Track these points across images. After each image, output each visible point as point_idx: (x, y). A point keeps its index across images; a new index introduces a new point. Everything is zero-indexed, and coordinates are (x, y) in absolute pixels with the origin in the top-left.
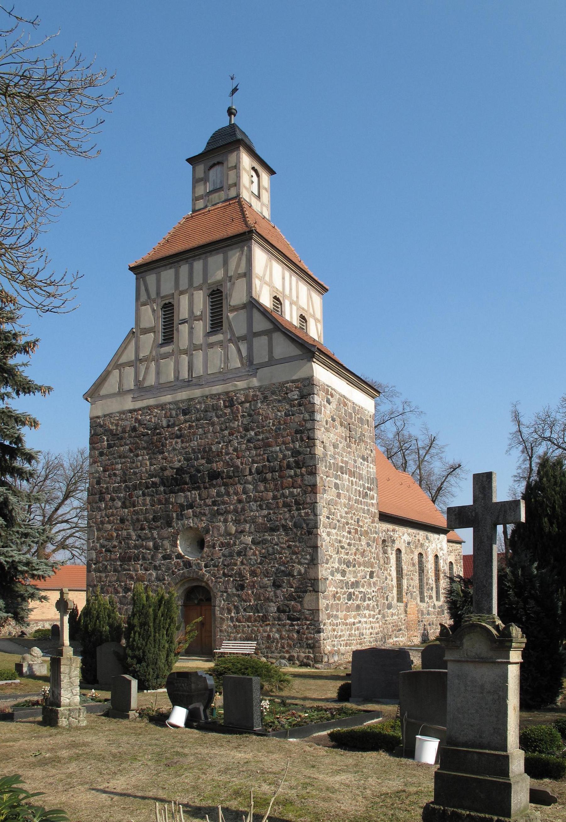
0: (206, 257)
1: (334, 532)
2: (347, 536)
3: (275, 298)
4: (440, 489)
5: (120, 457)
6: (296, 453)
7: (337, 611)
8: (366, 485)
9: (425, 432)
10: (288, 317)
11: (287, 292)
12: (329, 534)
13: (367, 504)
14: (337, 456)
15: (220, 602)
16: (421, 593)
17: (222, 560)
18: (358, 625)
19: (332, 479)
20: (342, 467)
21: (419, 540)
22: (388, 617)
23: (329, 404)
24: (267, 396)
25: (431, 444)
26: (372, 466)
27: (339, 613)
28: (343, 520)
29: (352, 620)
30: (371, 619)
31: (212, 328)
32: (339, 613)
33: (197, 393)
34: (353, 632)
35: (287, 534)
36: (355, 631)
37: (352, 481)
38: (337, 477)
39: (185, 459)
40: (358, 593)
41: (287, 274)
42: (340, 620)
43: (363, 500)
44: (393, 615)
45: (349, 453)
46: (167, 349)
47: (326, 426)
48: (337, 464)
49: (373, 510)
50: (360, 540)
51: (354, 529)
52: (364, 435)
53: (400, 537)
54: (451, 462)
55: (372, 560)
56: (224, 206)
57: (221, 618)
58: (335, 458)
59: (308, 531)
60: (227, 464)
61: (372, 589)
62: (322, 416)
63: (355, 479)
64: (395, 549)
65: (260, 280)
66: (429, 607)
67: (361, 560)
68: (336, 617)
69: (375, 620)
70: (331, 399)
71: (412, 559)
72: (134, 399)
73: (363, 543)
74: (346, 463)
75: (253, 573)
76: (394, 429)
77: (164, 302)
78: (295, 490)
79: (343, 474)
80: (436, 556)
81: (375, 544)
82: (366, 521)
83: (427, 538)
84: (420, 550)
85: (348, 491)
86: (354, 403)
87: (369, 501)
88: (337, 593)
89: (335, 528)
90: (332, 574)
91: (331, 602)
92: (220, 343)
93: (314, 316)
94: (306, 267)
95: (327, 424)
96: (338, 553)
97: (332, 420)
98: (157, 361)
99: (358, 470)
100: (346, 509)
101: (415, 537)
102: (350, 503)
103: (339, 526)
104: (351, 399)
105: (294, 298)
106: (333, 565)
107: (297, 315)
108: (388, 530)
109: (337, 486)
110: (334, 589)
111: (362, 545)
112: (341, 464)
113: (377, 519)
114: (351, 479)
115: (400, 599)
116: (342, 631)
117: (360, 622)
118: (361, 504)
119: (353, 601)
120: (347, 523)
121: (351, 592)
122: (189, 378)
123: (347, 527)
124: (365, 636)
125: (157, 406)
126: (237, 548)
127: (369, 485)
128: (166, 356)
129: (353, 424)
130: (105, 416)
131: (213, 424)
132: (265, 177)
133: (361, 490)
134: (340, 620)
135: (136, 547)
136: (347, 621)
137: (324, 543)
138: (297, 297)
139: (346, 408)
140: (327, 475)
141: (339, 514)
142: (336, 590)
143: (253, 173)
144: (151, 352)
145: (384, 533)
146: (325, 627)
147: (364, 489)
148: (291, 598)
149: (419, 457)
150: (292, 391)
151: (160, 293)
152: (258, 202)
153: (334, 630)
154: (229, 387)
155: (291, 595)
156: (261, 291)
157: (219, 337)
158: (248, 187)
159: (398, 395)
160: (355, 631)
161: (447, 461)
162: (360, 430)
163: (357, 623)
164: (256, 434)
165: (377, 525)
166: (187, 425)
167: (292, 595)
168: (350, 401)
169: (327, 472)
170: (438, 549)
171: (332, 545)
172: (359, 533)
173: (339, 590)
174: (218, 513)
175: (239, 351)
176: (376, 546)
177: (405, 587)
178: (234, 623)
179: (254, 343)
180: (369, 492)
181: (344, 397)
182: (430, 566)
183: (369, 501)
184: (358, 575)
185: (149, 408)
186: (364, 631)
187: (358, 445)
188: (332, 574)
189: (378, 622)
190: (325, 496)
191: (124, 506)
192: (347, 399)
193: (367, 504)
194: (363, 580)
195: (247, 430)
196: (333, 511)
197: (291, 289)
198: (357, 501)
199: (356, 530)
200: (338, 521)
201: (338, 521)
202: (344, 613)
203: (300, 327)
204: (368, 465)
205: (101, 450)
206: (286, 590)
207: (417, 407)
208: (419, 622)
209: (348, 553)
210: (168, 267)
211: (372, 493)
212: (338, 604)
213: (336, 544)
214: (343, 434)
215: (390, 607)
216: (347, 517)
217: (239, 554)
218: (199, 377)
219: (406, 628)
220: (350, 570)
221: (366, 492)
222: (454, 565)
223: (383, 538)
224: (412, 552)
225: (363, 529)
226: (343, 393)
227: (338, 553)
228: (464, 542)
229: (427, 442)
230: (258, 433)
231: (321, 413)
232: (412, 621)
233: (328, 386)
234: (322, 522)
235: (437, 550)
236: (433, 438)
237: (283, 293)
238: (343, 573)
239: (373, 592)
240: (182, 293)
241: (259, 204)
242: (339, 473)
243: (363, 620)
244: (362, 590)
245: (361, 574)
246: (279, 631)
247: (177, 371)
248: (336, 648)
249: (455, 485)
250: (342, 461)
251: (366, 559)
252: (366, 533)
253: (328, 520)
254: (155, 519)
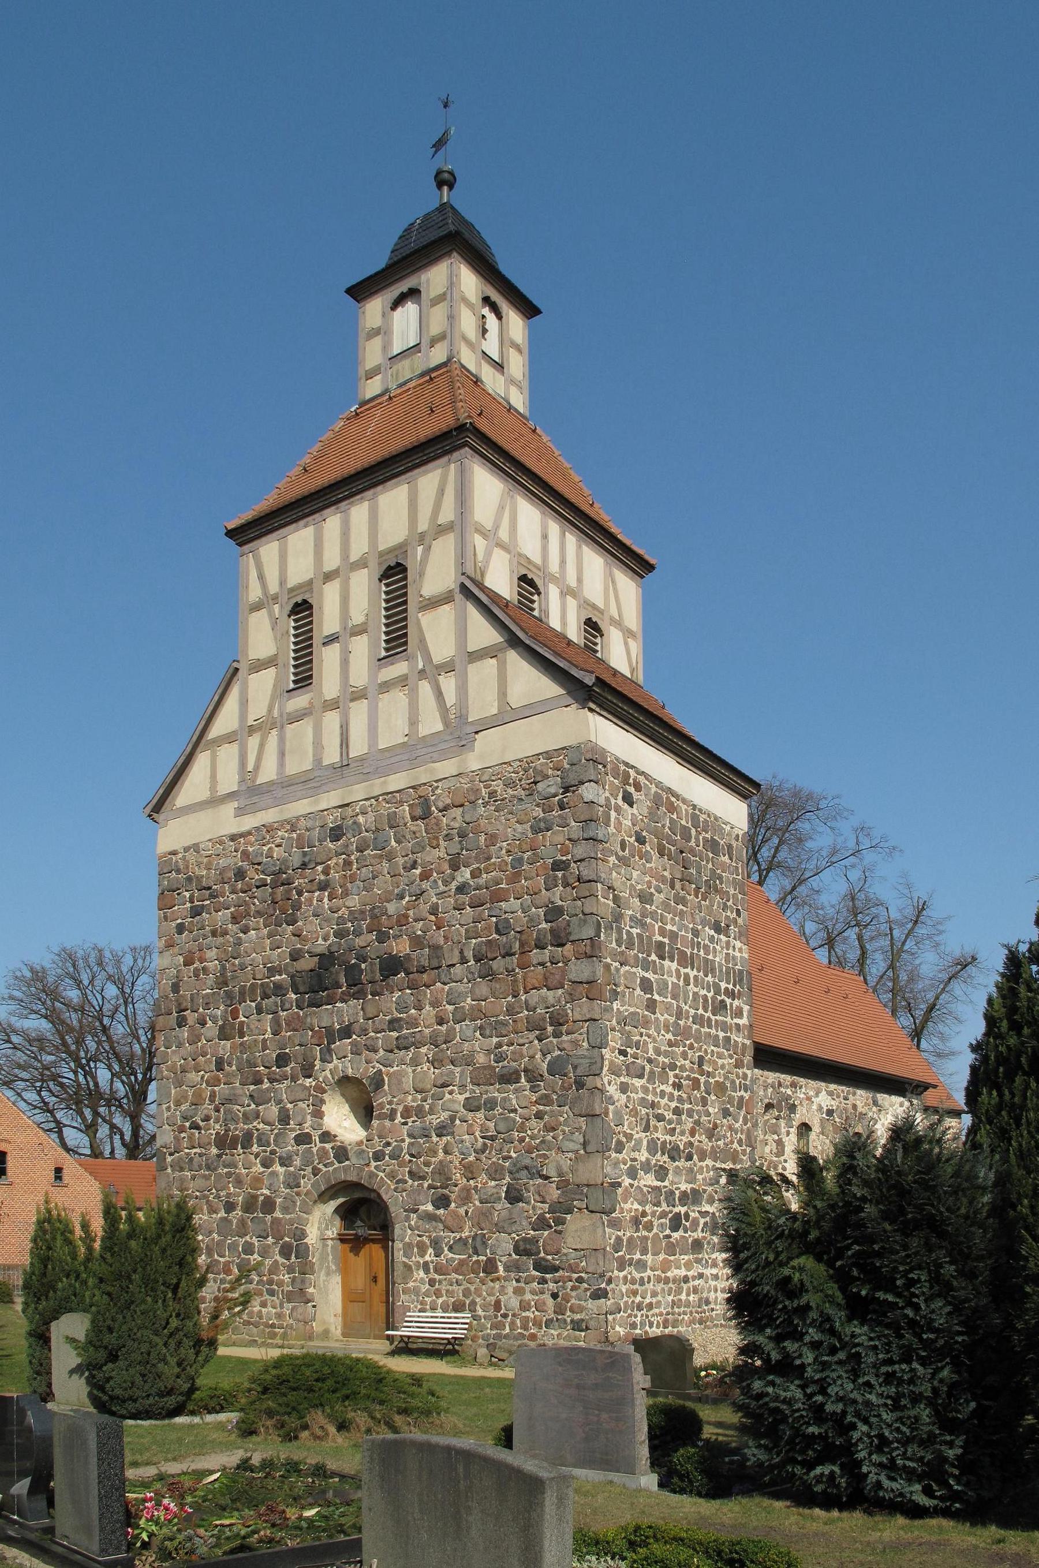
0: (375, 496)
1: (637, 1084)
2: (671, 1094)
3: (523, 578)
4: (932, 1008)
5: (214, 934)
6: (554, 913)
7: (644, 1252)
8: (723, 985)
9: (906, 891)
10: (555, 623)
11: (554, 567)
12: (624, 1088)
13: (725, 1027)
14: (649, 920)
15: (404, 1233)
17: (406, 1143)
18: (697, 1282)
19: (634, 970)
20: (660, 945)
21: (855, 1107)
23: (631, 805)
24: (496, 792)
25: (918, 916)
26: (738, 944)
27: (649, 1258)
28: (661, 1059)
29: (682, 1272)
31: (387, 650)
32: (649, 1258)
33: (358, 792)
34: (683, 1297)
35: (534, 1089)
36: (688, 1295)
37: (687, 976)
38: (646, 966)
39: (337, 934)
40: (697, 1215)
41: (554, 528)
42: (649, 1272)
43: (713, 1018)
45: (682, 914)
46: (300, 701)
47: (621, 853)
48: (649, 938)
49: (739, 1040)
50: (704, 1102)
51: (688, 1078)
52: (720, 878)
53: (809, 1099)
54: (957, 953)
55: (735, 1145)
56: (420, 385)
57: (406, 1265)
58: (643, 925)
59: (576, 1082)
60: (417, 942)
62: (612, 829)
63: (695, 972)
64: (796, 1124)
65: (484, 535)
67: (707, 1145)
68: (641, 1265)
70: (636, 795)
72: (240, 812)
73: (711, 1110)
74: (673, 936)
75: (470, 1172)
76: (842, 888)
77: (294, 601)
78: (550, 993)
79: (663, 959)
81: (743, 1113)
82: (720, 1062)
83: (875, 1103)
85: (675, 997)
86: (694, 807)
87: (728, 1019)
88: (644, 1214)
89: (641, 1076)
90: (632, 1174)
91: (628, 1234)
92: (402, 681)
93: (618, 624)
94: (606, 518)
95: (623, 850)
96: (646, 1129)
97: (637, 840)
98: (282, 727)
99: (702, 953)
100: (670, 1036)
101: (846, 1099)
102: (682, 1023)
103: (652, 1072)
104: (686, 796)
105: (572, 581)
106: (636, 1155)
107: (578, 619)
108: (780, 1085)
109: (646, 986)
110: (636, 1206)
111: (709, 1115)
112: (661, 939)
113: (748, 1059)
114: (683, 971)
116: (654, 1294)
117: (701, 1276)
118: (710, 1027)
119: (686, 1231)
120: (673, 1067)
121: (678, 1214)
122: (342, 761)
123: (671, 1074)
124: (712, 1306)
125: (282, 823)
126: (434, 1120)
127: (731, 987)
128: (296, 718)
129: (692, 851)
130: (186, 849)
131: (390, 857)
132: (516, 323)
133: (710, 995)
134: (649, 1272)
135: (246, 1118)
136: (669, 1274)
137: (611, 1107)
138: (580, 580)
139: (675, 816)
140: (622, 960)
141: (651, 1046)
142: (640, 1208)
143: (486, 311)
144: (270, 710)
145: (770, 1090)
146: (612, 1286)
147: (718, 992)
148: (541, 1224)
149: (892, 945)
150: (546, 777)
151: (285, 581)
152: (498, 375)
153: (635, 1293)
154: (422, 775)
155: (541, 1218)
156: (487, 562)
157: (399, 668)
158: (474, 340)
159: (845, 814)
160: (688, 1295)
161: (948, 950)
162: (710, 866)
163: (694, 1278)
164: (474, 875)
165: (749, 1072)
166: (341, 861)
167: (545, 1218)
168: (684, 801)
169: (622, 953)
171: (634, 1113)
172: (703, 1088)
173: (648, 1208)
174: (402, 1046)
175: (439, 694)
176: (745, 1118)
178: (430, 1276)
179: (469, 675)
180: (728, 1001)
181: (670, 791)
183: (728, 1019)
184: (699, 1177)
185: (269, 829)
186: (712, 1295)
187: (704, 899)
188: (632, 1174)
190: (615, 1006)
191: (224, 1036)
192: (677, 796)
193: (725, 1027)
195: (455, 866)
196: (638, 1038)
197: (563, 562)
198: (698, 1020)
199: (696, 1082)
200: (650, 1061)
201: (650, 1061)
202: (662, 1256)
203: (585, 645)
204: (728, 943)
205: (179, 921)
206: (534, 1207)
207: (884, 838)
209: (674, 1129)
210: (302, 523)
211: (736, 1003)
212: (646, 1238)
213: (644, 1111)
214: (666, 874)
216: (673, 1052)
217: (442, 1130)
218: (361, 759)
220: (677, 1167)
221: (723, 1001)
223: (767, 1101)
225: (711, 1080)
226: (667, 783)
227: (646, 1129)
229: (910, 912)
230: (477, 872)
231: (608, 824)
233: (627, 764)
234: (606, 1063)
236: (921, 904)
237: (543, 568)
238: (661, 1173)
240: (328, 577)
241: (501, 379)
242: (654, 957)
243: (709, 1272)
245: (705, 1174)
246: (518, 1291)
247: (318, 745)
248: (638, 1331)
249: (964, 998)
250: (662, 932)
251: (721, 1143)
252: (721, 1088)
253: (622, 1058)
254: (282, 1060)
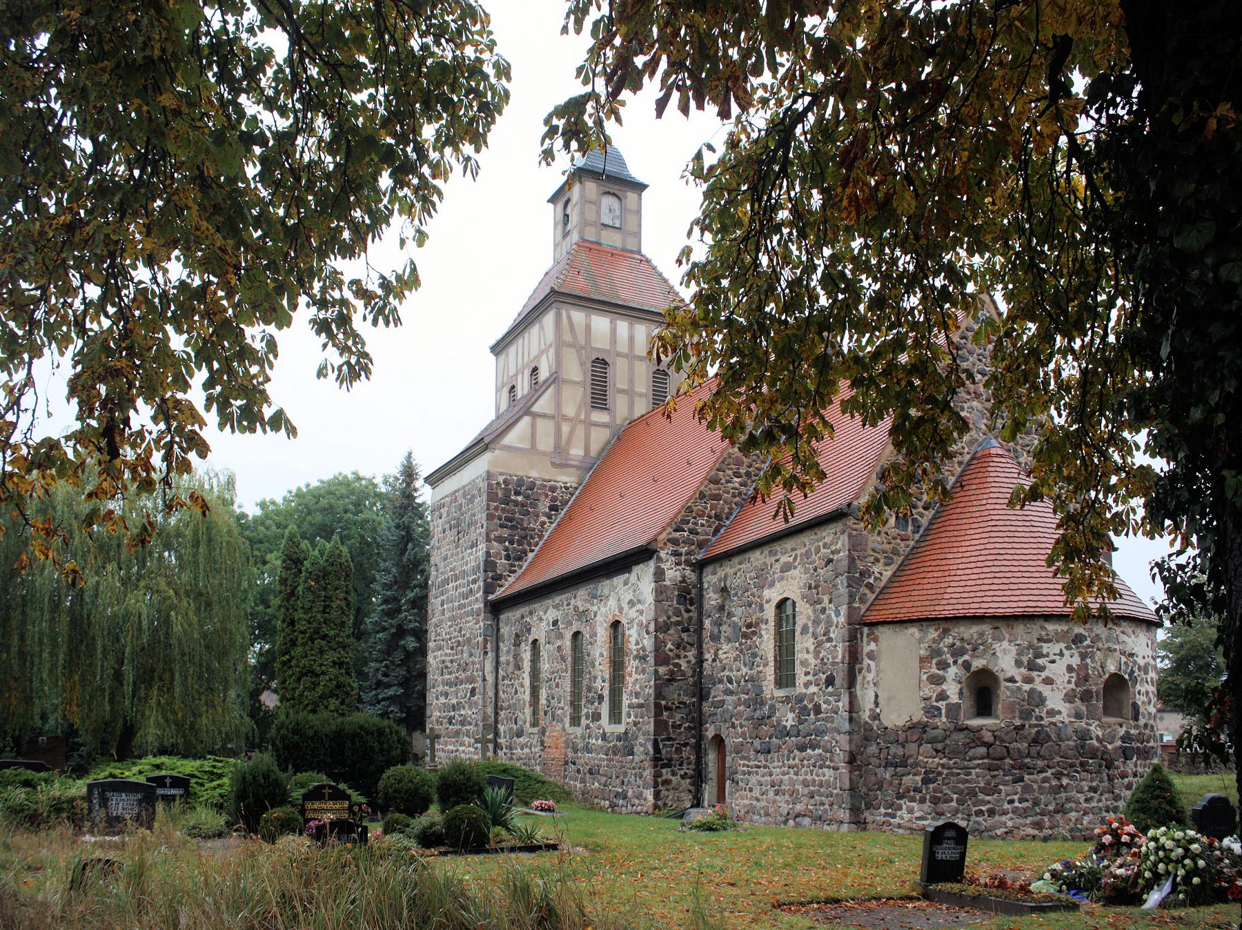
12: (435, 657)
16: (575, 706)
115: (534, 725)
177: (543, 701)
182: (599, 651)
208: (566, 763)
215: (519, 734)
238: (446, 695)
244: (463, 712)
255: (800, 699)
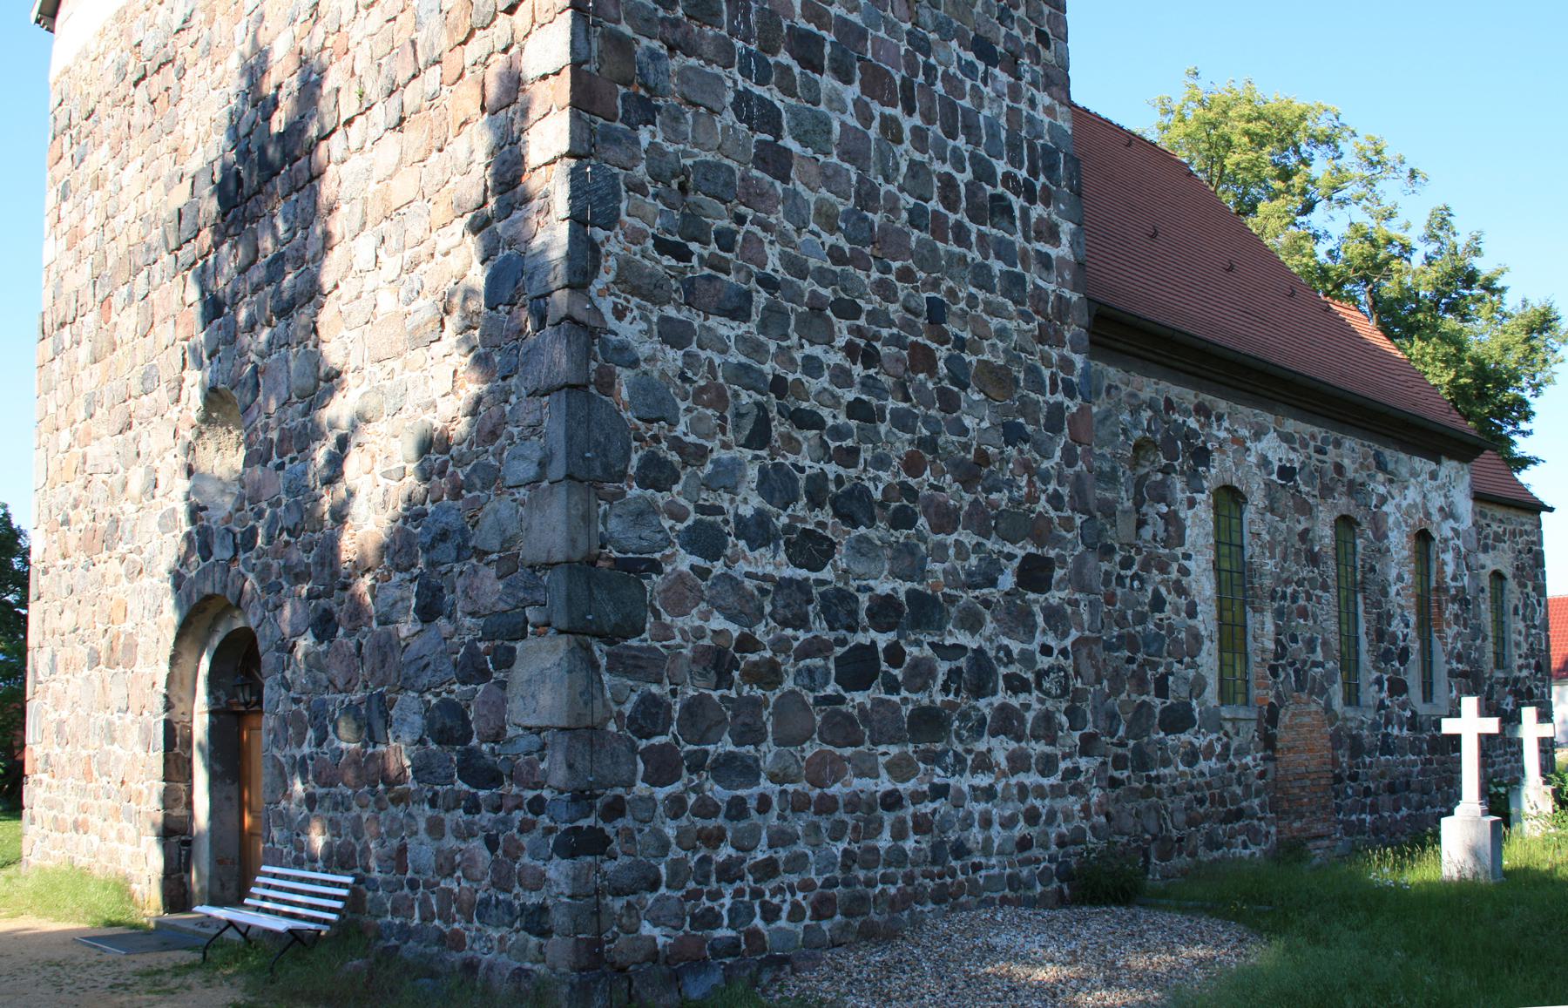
21: (1339, 468)
22: (1166, 763)
30: (1031, 779)
44: (1192, 757)
55: (1042, 505)
61: (1039, 638)
66: (1388, 722)
69: (1054, 780)
71: (1304, 535)
80: (1423, 537)
83: (1381, 466)
84: (1343, 503)
170: (1434, 511)
186: (976, 835)
189: (1077, 790)
194: (967, 597)
208: (1338, 779)
212: (757, 704)
219: (1273, 806)
222: (1512, 584)
224: (1305, 509)
228: (1551, 510)
232: (1301, 777)
235: (1428, 515)
239: (1046, 650)
255: (1517, 680)
